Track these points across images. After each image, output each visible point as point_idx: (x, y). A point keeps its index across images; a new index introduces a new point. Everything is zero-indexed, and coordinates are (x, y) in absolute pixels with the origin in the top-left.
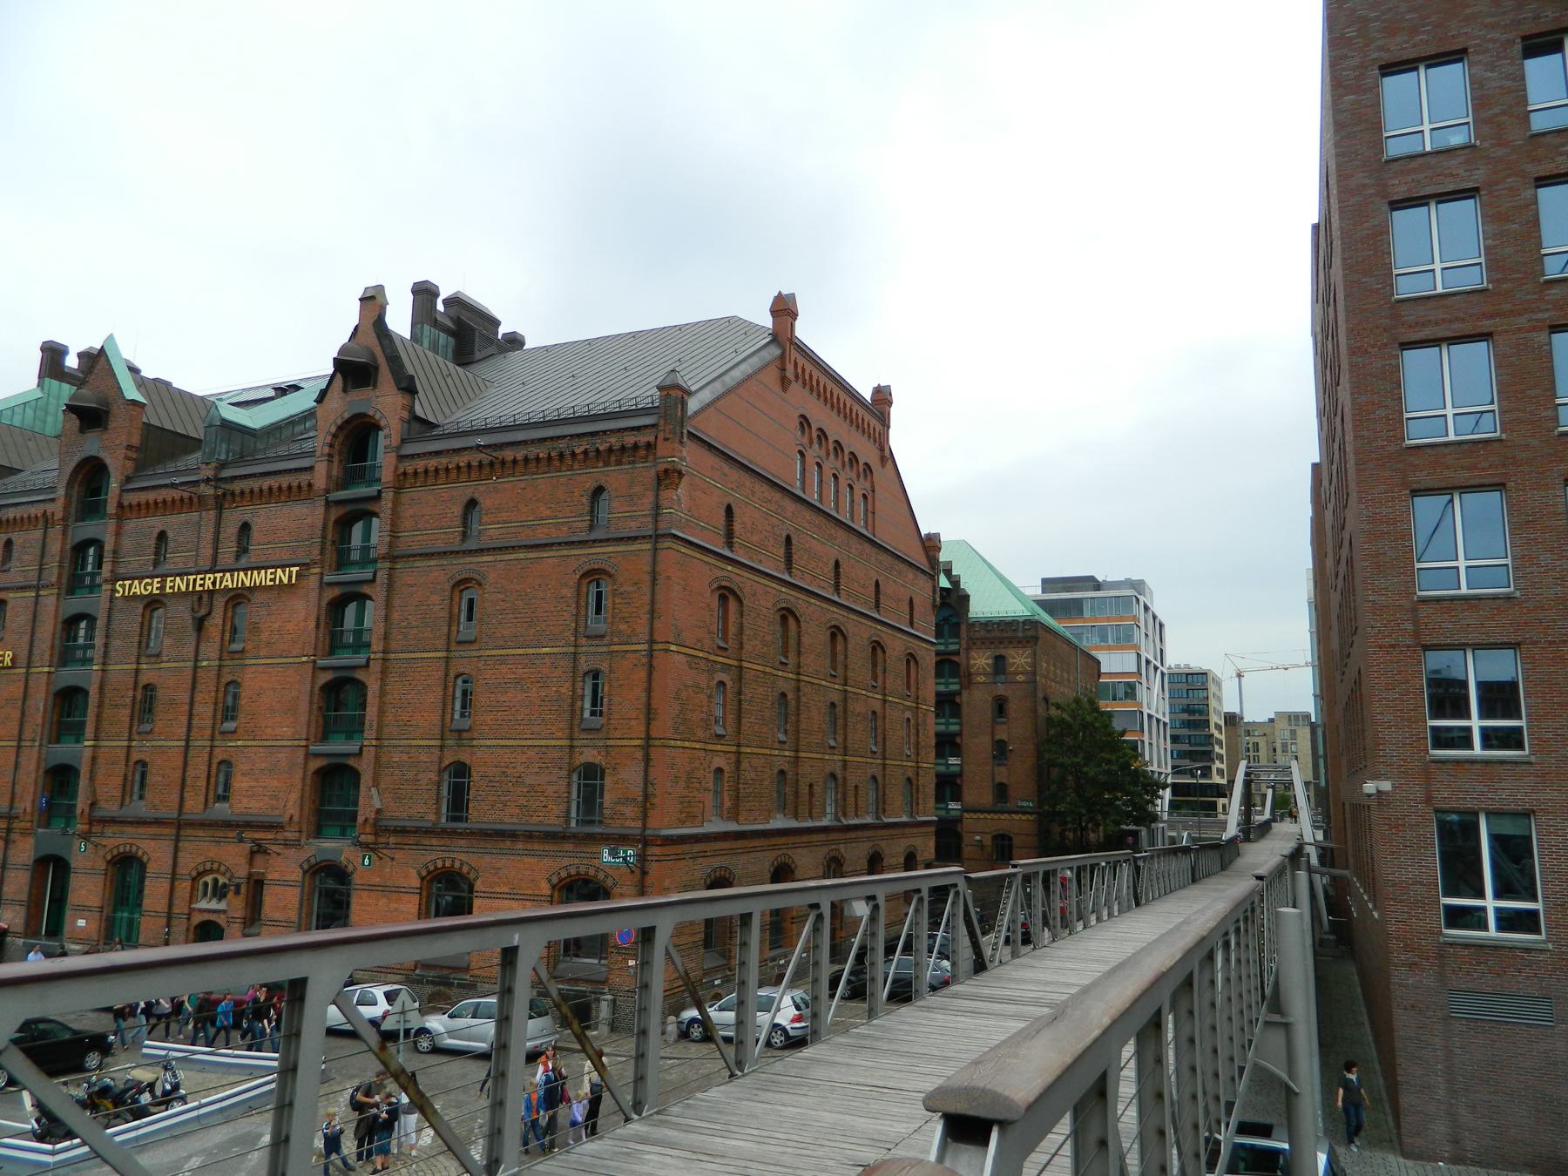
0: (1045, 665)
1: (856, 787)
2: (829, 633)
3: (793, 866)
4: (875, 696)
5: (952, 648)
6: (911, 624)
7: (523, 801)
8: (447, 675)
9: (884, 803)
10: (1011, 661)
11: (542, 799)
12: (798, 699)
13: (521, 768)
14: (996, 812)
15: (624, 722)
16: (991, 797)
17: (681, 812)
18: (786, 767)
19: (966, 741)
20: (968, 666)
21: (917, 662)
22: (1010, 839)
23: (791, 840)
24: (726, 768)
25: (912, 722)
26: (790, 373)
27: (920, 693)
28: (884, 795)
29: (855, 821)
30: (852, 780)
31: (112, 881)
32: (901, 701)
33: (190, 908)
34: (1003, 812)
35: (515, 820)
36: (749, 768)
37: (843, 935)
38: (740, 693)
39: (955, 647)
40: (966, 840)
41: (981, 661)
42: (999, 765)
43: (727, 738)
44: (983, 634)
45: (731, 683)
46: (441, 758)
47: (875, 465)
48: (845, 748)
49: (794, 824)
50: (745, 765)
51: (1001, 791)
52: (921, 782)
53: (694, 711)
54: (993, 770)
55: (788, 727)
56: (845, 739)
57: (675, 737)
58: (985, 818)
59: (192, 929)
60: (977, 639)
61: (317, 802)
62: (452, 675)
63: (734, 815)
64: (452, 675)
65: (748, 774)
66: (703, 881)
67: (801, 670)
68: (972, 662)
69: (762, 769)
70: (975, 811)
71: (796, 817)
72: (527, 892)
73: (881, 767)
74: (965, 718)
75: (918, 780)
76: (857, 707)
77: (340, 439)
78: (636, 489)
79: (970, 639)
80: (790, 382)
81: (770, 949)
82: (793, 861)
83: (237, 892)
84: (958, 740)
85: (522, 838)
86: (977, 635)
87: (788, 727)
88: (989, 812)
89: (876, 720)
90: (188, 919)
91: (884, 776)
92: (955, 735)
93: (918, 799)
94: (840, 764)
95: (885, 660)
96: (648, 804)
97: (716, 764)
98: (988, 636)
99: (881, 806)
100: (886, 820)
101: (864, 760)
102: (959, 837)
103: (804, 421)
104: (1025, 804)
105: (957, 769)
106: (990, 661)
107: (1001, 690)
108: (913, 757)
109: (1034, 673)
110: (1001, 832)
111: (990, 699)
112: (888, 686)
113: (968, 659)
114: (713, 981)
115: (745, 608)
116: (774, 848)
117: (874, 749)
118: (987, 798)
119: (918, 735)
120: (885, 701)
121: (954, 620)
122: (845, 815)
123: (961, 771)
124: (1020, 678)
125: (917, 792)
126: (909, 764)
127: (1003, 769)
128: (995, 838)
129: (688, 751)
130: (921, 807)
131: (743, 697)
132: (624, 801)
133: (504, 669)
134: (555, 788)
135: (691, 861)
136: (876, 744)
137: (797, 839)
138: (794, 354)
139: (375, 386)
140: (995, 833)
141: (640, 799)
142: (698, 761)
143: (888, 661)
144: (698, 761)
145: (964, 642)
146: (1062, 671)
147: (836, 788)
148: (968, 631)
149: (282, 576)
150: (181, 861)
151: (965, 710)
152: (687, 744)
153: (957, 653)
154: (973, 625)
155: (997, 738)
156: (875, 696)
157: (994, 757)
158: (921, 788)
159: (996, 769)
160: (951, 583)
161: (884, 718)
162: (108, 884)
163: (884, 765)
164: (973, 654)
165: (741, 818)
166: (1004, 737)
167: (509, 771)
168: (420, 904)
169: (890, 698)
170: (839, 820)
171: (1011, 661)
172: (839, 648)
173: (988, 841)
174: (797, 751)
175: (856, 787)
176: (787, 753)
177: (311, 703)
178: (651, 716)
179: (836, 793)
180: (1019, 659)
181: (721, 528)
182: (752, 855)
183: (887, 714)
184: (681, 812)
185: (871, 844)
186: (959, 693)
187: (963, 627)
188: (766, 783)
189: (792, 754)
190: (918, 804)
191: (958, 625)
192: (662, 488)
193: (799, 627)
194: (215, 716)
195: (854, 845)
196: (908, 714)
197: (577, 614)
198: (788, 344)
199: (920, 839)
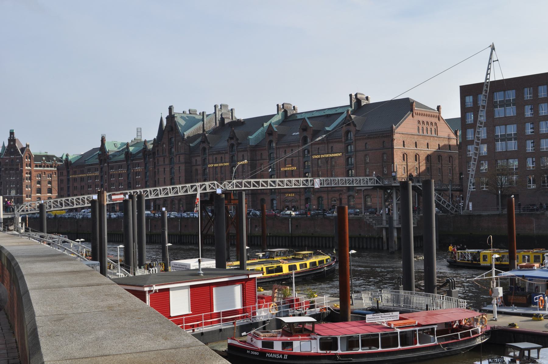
21: (452, 157)
52: (454, 181)
95: (442, 158)
112: (443, 163)
149: (339, 155)
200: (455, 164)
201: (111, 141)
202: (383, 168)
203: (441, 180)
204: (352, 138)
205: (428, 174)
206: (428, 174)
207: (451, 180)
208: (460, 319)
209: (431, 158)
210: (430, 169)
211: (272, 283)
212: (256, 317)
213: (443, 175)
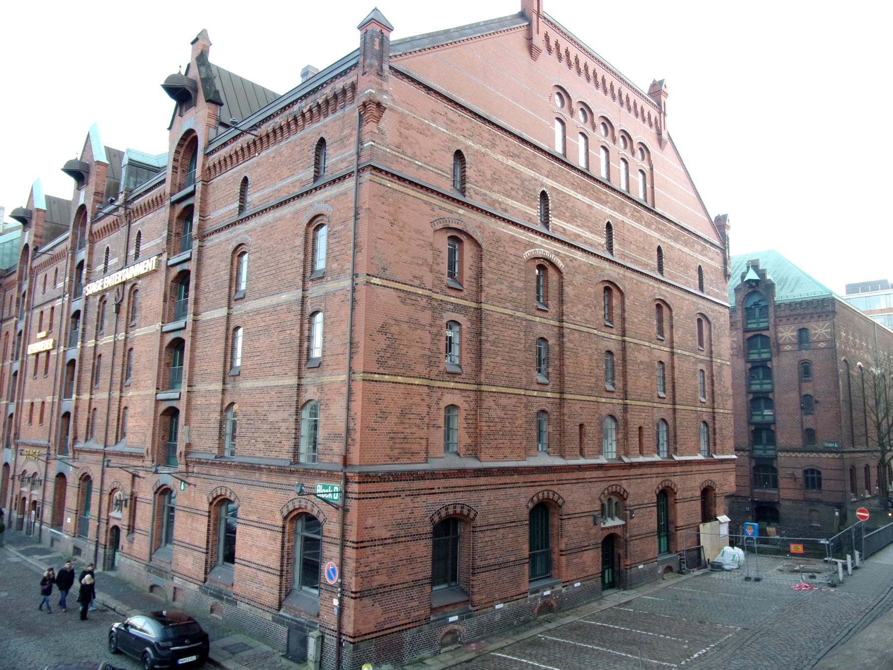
0: (843, 334)
1: (640, 428)
2: (602, 287)
3: (560, 501)
4: (662, 348)
5: (762, 325)
6: (701, 288)
7: (267, 437)
8: (227, 329)
9: (676, 443)
10: (813, 332)
11: (279, 435)
12: (561, 345)
13: (266, 408)
14: (805, 452)
15: (334, 358)
16: (801, 440)
17: (392, 449)
18: (549, 407)
19: (778, 397)
20: (776, 338)
21: (709, 322)
22: (819, 473)
23: (555, 476)
24: (463, 406)
25: (706, 373)
26: (539, 41)
27: (714, 349)
28: (675, 436)
29: (641, 459)
30: (635, 421)
31: (82, 492)
32: (692, 354)
33: (108, 515)
34: (812, 452)
35: (262, 455)
36: (495, 407)
37: (628, 562)
38: (479, 334)
39: (765, 325)
40: (781, 472)
41: (787, 333)
42: (807, 414)
43: (463, 376)
44: (787, 312)
45: (469, 324)
46: (222, 400)
47: (653, 147)
48: (625, 392)
49: (558, 461)
50: (488, 402)
51: (810, 435)
52: (717, 426)
53: (410, 347)
54: (802, 419)
55: (550, 370)
56: (625, 385)
57: (381, 370)
58: (796, 457)
59: (109, 530)
60: (783, 317)
61: (167, 438)
62: (231, 328)
63: (474, 452)
64: (231, 328)
65: (492, 409)
66: (427, 519)
67: (565, 318)
68: (780, 335)
69: (513, 408)
70: (788, 451)
71: (562, 456)
72: (267, 522)
73: (671, 412)
74: (775, 380)
75: (714, 424)
76: (637, 357)
77: (182, 151)
78: (346, 132)
79: (776, 317)
80: (539, 51)
81: (530, 582)
82: (560, 497)
83: (126, 506)
84: (771, 396)
85: (265, 472)
86: (783, 314)
87: (550, 370)
88: (800, 452)
89: (663, 369)
90: (107, 523)
91: (675, 419)
92: (767, 392)
93: (715, 439)
94: (620, 407)
95: (671, 317)
96: (350, 440)
97: (448, 399)
98: (792, 313)
99: (673, 445)
100: (677, 458)
101: (650, 404)
102: (775, 470)
103: (562, 93)
104: (830, 445)
105: (770, 419)
106: (795, 334)
107: (805, 355)
108: (708, 403)
109: (833, 341)
110: (811, 468)
111: (796, 363)
112: (676, 339)
113: (776, 333)
114: (446, 618)
115: (484, 252)
116: (533, 484)
117: (662, 395)
118: (797, 441)
119: (713, 385)
120: (672, 353)
121: (763, 304)
122: (626, 454)
123: (775, 418)
124: (822, 345)
125: (715, 434)
126: (704, 410)
127: (809, 417)
128: (806, 472)
129: (402, 386)
130: (718, 447)
131: (483, 338)
132: (335, 437)
133: (258, 318)
134: (287, 424)
135: (408, 499)
136: (664, 391)
137: (565, 476)
138: (544, 28)
139: (195, 105)
140: (806, 468)
141: (344, 435)
142: (419, 398)
143: (675, 318)
144: (419, 398)
145: (772, 320)
146: (861, 340)
147: (617, 428)
148: (775, 311)
150: (106, 481)
151: (775, 372)
152: (400, 379)
153: (767, 329)
154: (779, 305)
155: (804, 393)
156: (662, 348)
157: (802, 408)
158: (718, 430)
159: (804, 417)
160: (759, 275)
161: (673, 368)
162: (80, 493)
163: (674, 410)
164: (780, 329)
165: (483, 456)
166: (810, 392)
167: (259, 409)
168: (209, 525)
169: (679, 351)
170: (620, 459)
171: (813, 332)
172: (615, 302)
173: (799, 474)
174: (562, 393)
175: (640, 428)
176: (549, 395)
177: (160, 360)
178: (354, 350)
179: (617, 433)
180: (819, 330)
181: (448, 170)
182: (502, 492)
183: (676, 365)
184: (392, 449)
185: (660, 480)
186: (770, 360)
187: (771, 309)
188: (520, 422)
189: (558, 396)
190: (715, 444)
191: (766, 307)
192: (364, 123)
193: (562, 278)
194: (122, 374)
195: (639, 480)
196: (701, 366)
197: (305, 261)
198: (534, 16)
199: (718, 475)
200: (719, 356)
201: (93, 196)
202: (307, 317)
203: (670, 422)
204: (755, 451)
205: (609, 387)
206: (609, 387)
207: (705, 423)
208: (392, 20)
209: (623, 303)
210: (617, 358)
211: (202, 461)
212: (364, 372)
213: (678, 398)
